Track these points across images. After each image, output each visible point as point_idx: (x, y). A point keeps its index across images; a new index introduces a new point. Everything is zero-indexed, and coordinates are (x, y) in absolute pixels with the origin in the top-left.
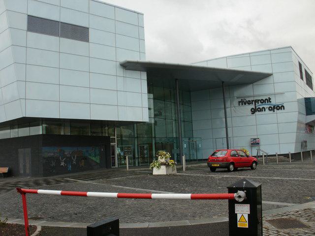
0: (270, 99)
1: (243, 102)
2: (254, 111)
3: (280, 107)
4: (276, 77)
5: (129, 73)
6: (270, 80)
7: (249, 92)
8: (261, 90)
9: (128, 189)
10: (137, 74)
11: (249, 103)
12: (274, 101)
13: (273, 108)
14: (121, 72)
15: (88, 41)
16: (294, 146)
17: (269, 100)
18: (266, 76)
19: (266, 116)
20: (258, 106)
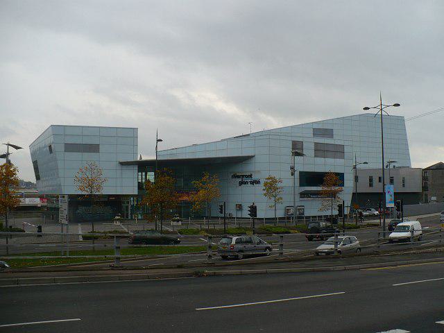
0: (251, 175)
1: (235, 176)
2: (241, 183)
3: (258, 182)
4: (257, 158)
5: (124, 167)
6: (253, 160)
7: (240, 170)
8: (240, 170)
9: (80, 255)
10: (131, 167)
11: (239, 177)
12: (255, 177)
13: (252, 183)
14: (119, 167)
15: (65, 151)
16: (378, 167)
17: (251, 176)
18: (253, 157)
19: (248, 188)
20: (246, 180)
